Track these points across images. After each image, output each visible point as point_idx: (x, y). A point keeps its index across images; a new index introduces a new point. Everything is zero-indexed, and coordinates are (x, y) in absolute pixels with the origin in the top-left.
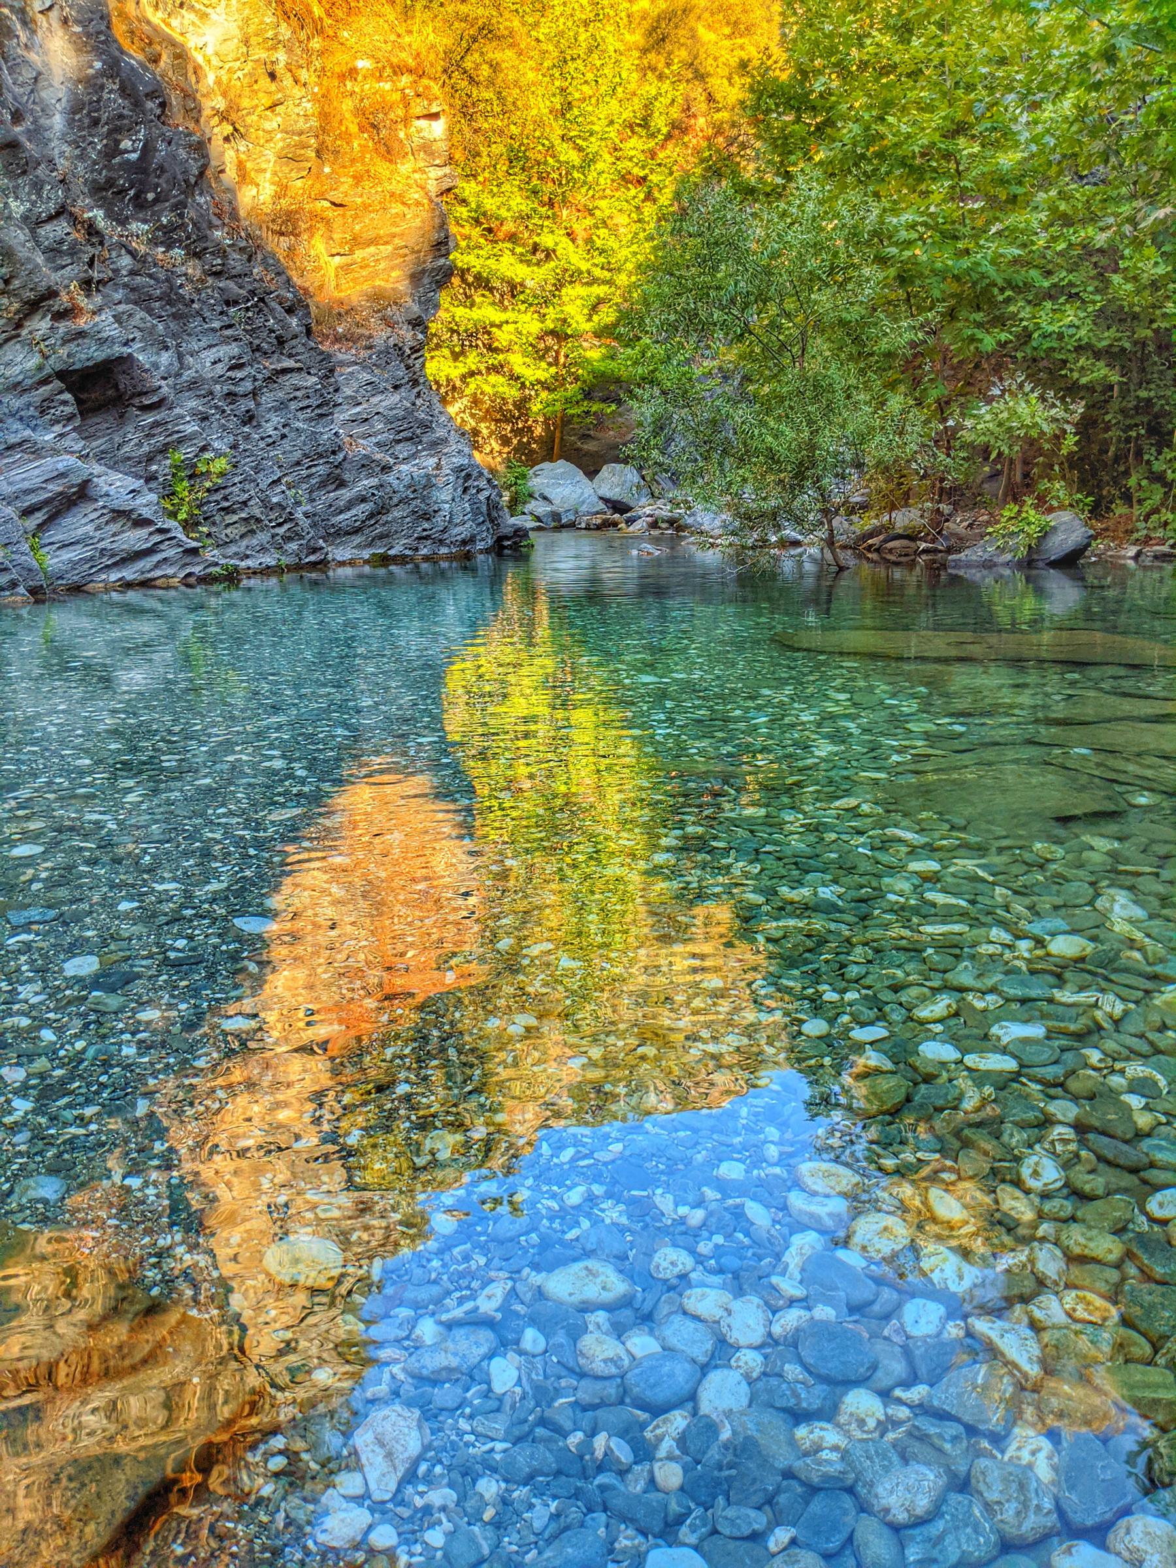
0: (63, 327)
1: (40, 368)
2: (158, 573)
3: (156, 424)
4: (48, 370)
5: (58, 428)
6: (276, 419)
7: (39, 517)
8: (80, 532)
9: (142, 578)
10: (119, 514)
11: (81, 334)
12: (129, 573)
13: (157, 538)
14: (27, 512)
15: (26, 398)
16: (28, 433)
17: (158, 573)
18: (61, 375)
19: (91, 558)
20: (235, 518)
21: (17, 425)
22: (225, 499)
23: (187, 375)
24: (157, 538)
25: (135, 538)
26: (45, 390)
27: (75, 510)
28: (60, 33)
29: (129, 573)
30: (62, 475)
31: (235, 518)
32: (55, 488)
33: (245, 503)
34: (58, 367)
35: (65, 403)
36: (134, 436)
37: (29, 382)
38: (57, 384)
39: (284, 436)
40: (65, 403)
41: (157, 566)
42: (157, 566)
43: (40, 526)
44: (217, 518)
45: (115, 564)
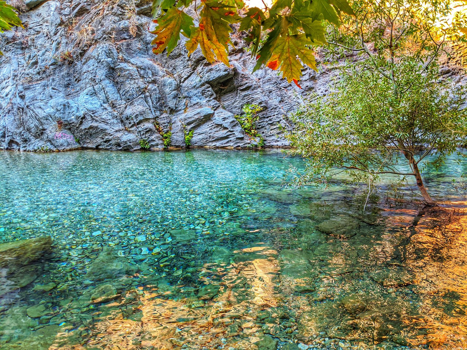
0: (207, 68)
1: (200, 81)
2: (228, 144)
3: (245, 96)
4: (203, 82)
5: (208, 99)
6: (323, 89)
7: (192, 125)
8: (205, 130)
9: (222, 146)
10: (218, 125)
11: (211, 70)
12: (218, 144)
13: (229, 133)
14: (189, 124)
15: (198, 90)
16: (199, 100)
17: (228, 144)
18: (208, 82)
19: (207, 138)
20: (275, 127)
21: (196, 98)
22: (270, 120)
23: (268, 77)
24: (229, 133)
25: (222, 133)
26: (203, 88)
27: (206, 124)
28: (80, 128)
29: (218, 144)
30: (198, 113)
31: (275, 127)
32: (196, 117)
33: (279, 122)
34: (206, 80)
35: (209, 91)
36: (238, 100)
37: (198, 85)
38: (207, 85)
39: (325, 95)
40: (209, 91)
41: (228, 142)
42: (228, 142)
43: (192, 128)
44: (267, 127)
45: (215, 141)
